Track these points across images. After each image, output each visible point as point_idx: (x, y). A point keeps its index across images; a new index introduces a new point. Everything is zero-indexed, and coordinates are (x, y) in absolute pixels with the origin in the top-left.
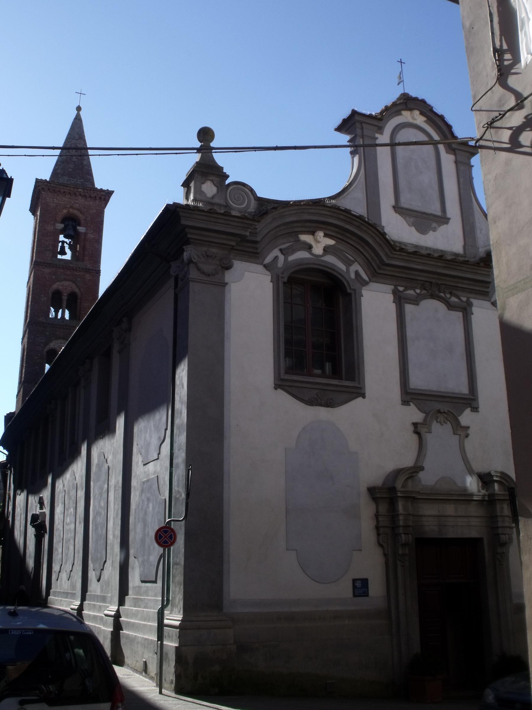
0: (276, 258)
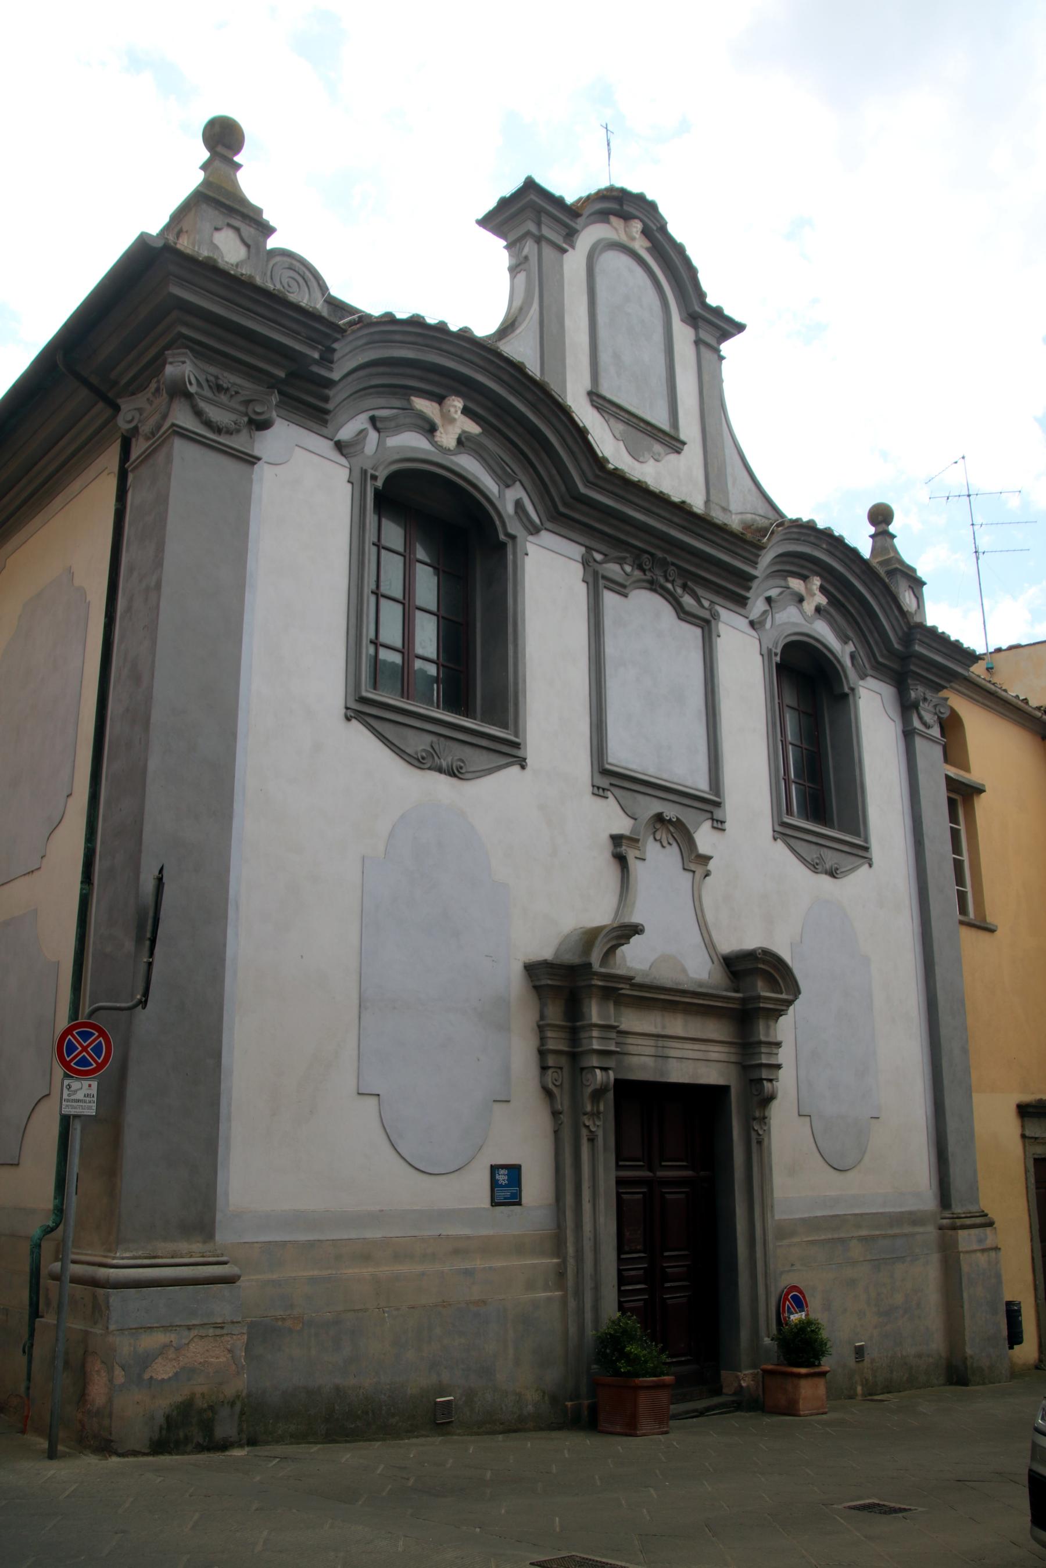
0: (362, 432)
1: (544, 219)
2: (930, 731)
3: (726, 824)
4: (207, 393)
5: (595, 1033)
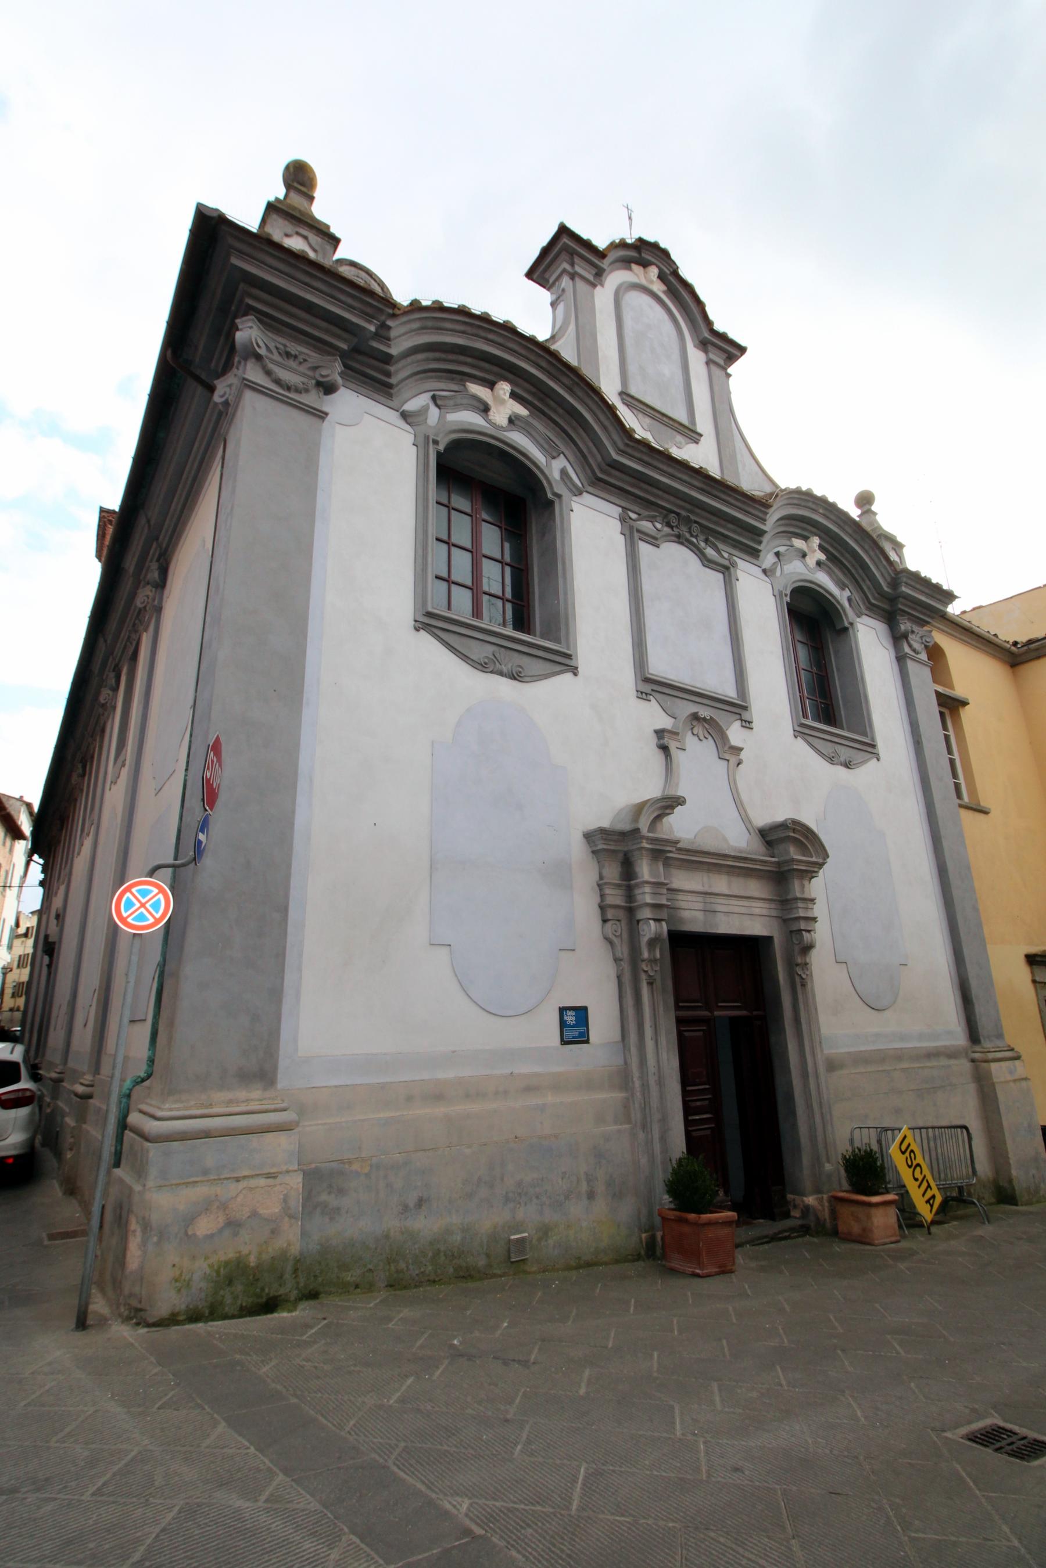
1: (577, 260)
2: (919, 656)
3: (753, 724)
4: (276, 357)
5: (647, 889)
